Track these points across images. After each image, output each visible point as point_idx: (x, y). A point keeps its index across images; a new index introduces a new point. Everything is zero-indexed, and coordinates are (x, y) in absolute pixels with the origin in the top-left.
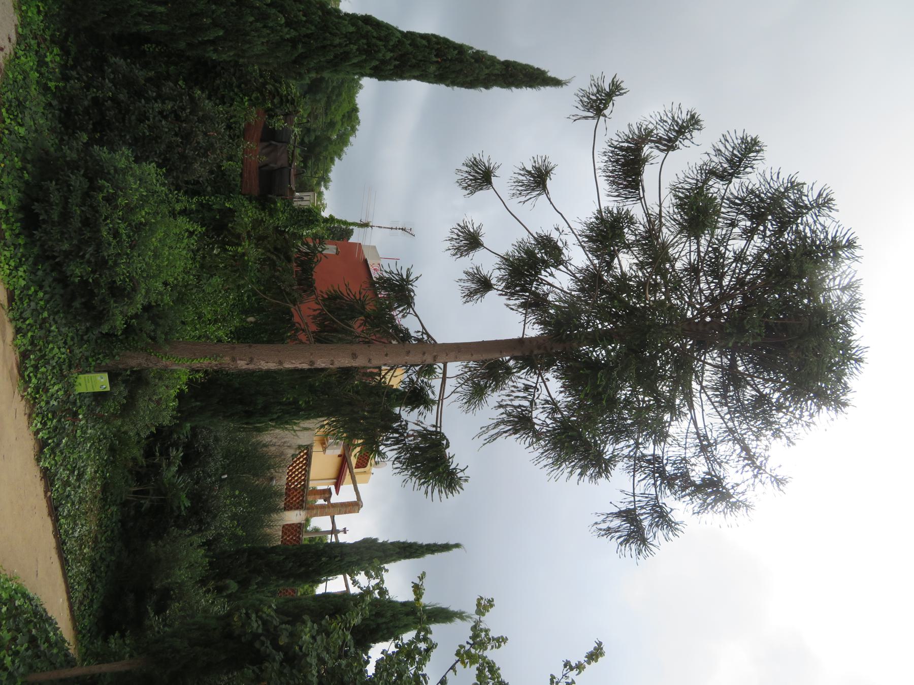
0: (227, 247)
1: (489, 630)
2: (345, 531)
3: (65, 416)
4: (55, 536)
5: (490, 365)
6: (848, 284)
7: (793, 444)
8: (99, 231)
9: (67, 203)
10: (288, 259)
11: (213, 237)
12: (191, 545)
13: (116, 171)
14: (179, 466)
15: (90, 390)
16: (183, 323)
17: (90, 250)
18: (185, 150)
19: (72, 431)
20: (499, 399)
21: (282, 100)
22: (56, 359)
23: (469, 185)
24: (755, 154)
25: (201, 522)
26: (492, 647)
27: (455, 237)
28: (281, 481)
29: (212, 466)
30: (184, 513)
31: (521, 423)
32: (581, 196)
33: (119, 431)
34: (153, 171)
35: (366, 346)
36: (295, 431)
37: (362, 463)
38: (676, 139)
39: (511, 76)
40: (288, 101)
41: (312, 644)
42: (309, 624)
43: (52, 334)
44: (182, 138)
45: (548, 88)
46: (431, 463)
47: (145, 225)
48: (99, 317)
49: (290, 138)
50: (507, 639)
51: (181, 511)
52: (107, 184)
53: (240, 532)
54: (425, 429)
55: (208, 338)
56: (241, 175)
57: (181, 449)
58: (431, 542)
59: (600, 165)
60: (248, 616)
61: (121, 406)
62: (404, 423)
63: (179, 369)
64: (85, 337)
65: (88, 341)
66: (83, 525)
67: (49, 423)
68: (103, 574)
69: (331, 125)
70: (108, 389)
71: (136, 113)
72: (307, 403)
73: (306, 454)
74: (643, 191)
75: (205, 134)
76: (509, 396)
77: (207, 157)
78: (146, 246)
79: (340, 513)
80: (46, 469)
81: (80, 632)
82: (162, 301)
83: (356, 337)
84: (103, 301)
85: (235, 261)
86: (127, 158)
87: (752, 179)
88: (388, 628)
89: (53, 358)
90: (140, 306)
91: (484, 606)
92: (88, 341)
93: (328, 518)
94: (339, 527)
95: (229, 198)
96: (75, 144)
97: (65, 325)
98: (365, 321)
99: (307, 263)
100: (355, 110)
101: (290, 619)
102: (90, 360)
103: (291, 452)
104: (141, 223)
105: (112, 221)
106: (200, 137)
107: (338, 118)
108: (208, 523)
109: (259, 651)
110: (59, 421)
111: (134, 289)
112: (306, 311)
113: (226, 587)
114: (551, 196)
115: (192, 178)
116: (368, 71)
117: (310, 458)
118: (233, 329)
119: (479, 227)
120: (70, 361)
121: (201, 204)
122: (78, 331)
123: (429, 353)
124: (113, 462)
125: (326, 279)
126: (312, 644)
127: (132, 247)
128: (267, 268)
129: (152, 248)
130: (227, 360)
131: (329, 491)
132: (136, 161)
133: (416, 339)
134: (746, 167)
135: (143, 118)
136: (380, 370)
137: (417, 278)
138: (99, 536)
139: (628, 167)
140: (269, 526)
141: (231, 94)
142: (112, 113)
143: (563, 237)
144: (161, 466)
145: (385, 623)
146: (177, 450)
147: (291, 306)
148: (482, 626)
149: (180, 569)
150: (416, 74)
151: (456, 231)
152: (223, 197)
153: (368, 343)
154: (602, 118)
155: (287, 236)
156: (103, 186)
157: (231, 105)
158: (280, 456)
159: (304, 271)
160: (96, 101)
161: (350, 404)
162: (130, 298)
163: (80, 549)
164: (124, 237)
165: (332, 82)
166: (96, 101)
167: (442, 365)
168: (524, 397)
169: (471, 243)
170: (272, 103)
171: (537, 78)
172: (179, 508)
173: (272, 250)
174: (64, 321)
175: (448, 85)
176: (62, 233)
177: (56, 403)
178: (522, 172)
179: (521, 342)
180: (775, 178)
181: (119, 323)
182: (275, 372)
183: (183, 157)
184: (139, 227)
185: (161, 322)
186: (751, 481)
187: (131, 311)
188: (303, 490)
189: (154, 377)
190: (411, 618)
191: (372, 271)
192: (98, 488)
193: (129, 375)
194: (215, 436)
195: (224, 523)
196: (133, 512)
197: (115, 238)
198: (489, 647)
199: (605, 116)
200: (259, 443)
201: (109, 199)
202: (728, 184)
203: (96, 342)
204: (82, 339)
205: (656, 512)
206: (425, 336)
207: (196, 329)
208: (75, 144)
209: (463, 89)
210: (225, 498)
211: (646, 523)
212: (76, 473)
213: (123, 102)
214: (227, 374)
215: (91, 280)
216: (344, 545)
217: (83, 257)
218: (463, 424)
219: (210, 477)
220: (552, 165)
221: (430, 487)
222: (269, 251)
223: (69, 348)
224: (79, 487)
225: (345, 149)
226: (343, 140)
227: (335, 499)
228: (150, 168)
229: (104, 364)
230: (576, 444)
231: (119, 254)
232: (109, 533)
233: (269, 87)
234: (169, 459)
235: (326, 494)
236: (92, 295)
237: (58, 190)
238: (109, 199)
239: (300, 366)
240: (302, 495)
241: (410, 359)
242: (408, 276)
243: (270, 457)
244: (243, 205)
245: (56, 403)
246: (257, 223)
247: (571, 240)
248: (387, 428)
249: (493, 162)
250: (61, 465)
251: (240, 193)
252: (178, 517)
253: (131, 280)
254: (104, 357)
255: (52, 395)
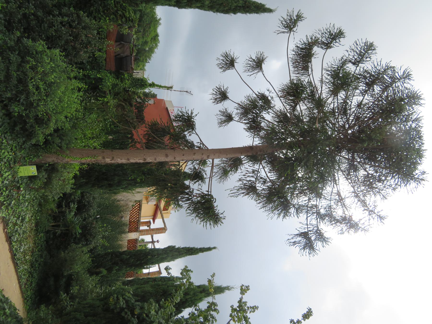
0: (99, 98)
1: (247, 302)
2: (158, 241)
3: (13, 189)
4: (10, 252)
5: (233, 159)
6: (415, 119)
7: (386, 199)
8: (28, 86)
9: (8, 69)
10: (131, 105)
11: (91, 94)
12: (83, 252)
13: (37, 53)
14: (75, 212)
15: (27, 175)
16: (76, 139)
17: (23, 97)
18: (75, 44)
19: (18, 196)
20: (240, 177)
21: (126, 19)
22: (7, 158)
23: (223, 67)
24: (371, 51)
25: (87, 240)
26: (250, 312)
27: (215, 93)
28: (126, 218)
29: (92, 211)
30: (78, 236)
31: (250, 189)
32: (277, 73)
33: (44, 195)
34: (58, 54)
35: (173, 150)
36: (133, 193)
37: (165, 209)
38: (331, 42)
39: (248, 7)
40: (130, 20)
41: (156, 316)
42: (154, 304)
43: (3, 145)
44: (73, 37)
45: (266, 14)
46: (206, 209)
47: (54, 83)
48: (29, 134)
49: (131, 40)
50: (258, 307)
51: (76, 235)
52: (31, 60)
53: (107, 244)
54: (202, 193)
55: (89, 147)
56: (105, 60)
57: (76, 204)
58: (202, 247)
59: (290, 56)
60: (118, 299)
61: (43, 182)
62: (191, 190)
63: (74, 163)
64: (23, 147)
65: (25, 148)
66: (25, 245)
67: (4, 193)
68: (37, 269)
69: (146, 43)
70: (36, 174)
71: (48, 22)
72: (141, 179)
73: (139, 204)
74: (312, 71)
75: (86, 36)
76: (244, 175)
77: (87, 48)
78: (55, 95)
79: (156, 233)
80: (4, 217)
81: (26, 299)
82: (64, 126)
83: (166, 146)
84: (31, 126)
85: (103, 105)
86: (43, 46)
87: (367, 66)
88: (191, 301)
89: (5, 158)
90: (52, 129)
91: (244, 290)
92: (25, 148)
93: (150, 236)
94: (155, 239)
95: (99, 72)
96: (12, 37)
97: (11, 139)
98: (170, 138)
99: (140, 108)
100: (157, 35)
101: (140, 298)
102: (26, 158)
103: (131, 204)
104: (52, 82)
105: (35, 80)
106: (83, 37)
107: (149, 39)
108: (91, 241)
109: (124, 317)
110: (10, 192)
111: (49, 120)
112: (140, 133)
113: (100, 272)
114: (264, 73)
115: (79, 60)
116: (173, 3)
117: (141, 207)
118: (102, 142)
119: (227, 89)
120: (15, 159)
121: (84, 75)
122: (18, 143)
123: (204, 153)
124: (40, 211)
125: (150, 115)
126: (156, 316)
127: (47, 96)
128: (120, 110)
129: (58, 96)
130: (100, 158)
131: (150, 222)
132: (48, 48)
133: (198, 147)
134: (366, 58)
135: (51, 25)
136: (179, 163)
137: (196, 115)
138: (35, 249)
139: (304, 57)
140: (121, 241)
141: (99, 15)
142: (34, 22)
143: (271, 94)
144: (66, 212)
145: (190, 298)
146: (74, 204)
147: (133, 129)
148: (244, 300)
149: (77, 265)
150: (199, 5)
151: (215, 90)
152: (96, 71)
153: (173, 149)
154: (292, 33)
155: (130, 93)
156: (30, 61)
157: (99, 22)
158: (126, 206)
159: (139, 111)
160: (25, 16)
161: (164, 180)
162: (46, 125)
163: (24, 257)
164: (42, 90)
165: (146, 21)
166: (25, 16)
167: (211, 160)
168: (252, 176)
169: (222, 97)
170: (122, 21)
171: (260, 8)
172: (76, 233)
173: (122, 100)
174: (10, 138)
175: (214, 12)
176: (7, 87)
177: (7, 182)
178: (250, 60)
179: (250, 148)
180: (379, 64)
181: (41, 138)
182: (125, 164)
183: (74, 48)
184: (50, 85)
185: (64, 138)
186: (367, 218)
187: (48, 132)
188: (138, 222)
189: (61, 168)
190: (203, 294)
191: (170, 113)
192: (33, 225)
193: (48, 167)
194: (93, 197)
195: (99, 241)
196: (52, 236)
197: (37, 90)
198: (249, 312)
199: (293, 31)
200: (115, 200)
201: (33, 68)
202: (357, 67)
203: (29, 149)
204: (21, 147)
205: (318, 233)
206: (201, 145)
207: (83, 142)
208: (12, 37)
209: (222, 14)
210: (99, 228)
211: (313, 238)
212: (20, 218)
213: (40, 16)
214: (99, 165)
215: (24, 115)
216: (158, 250)
217: (19, 101)
218: (224, 190)
219: (91, 217)
220: (265, 56)
221: (205, 223)
222: (121, 101)
223: (14, 152)
224: (22, 225)
225: (152, 55)
226: (151, 51)
227: (153, 226)
228: (57, 51)
229: (33, 161)
230: (277, 198)
231: (40, 99)
232: (40, 247)
233: (120, 12)
234: (70, 209)
235: (148, 224)
236: (25, 123)
237: (3, 62)
238: (33, 68)
239: (138, 161)
240: (137, 225)
241: (195, 157)
242: (192, 113)
243: (121, 207)
244: (107, 76)
245: (7, 182)
246: (114, 86)
247: (274, 95)
248: (183, 193)
249: (235, 55)
250: (12, 215)
251: (105, 70)
252: (75, 238)
253: (47, 115)
254: (34, 157)
255: (5, 178)
